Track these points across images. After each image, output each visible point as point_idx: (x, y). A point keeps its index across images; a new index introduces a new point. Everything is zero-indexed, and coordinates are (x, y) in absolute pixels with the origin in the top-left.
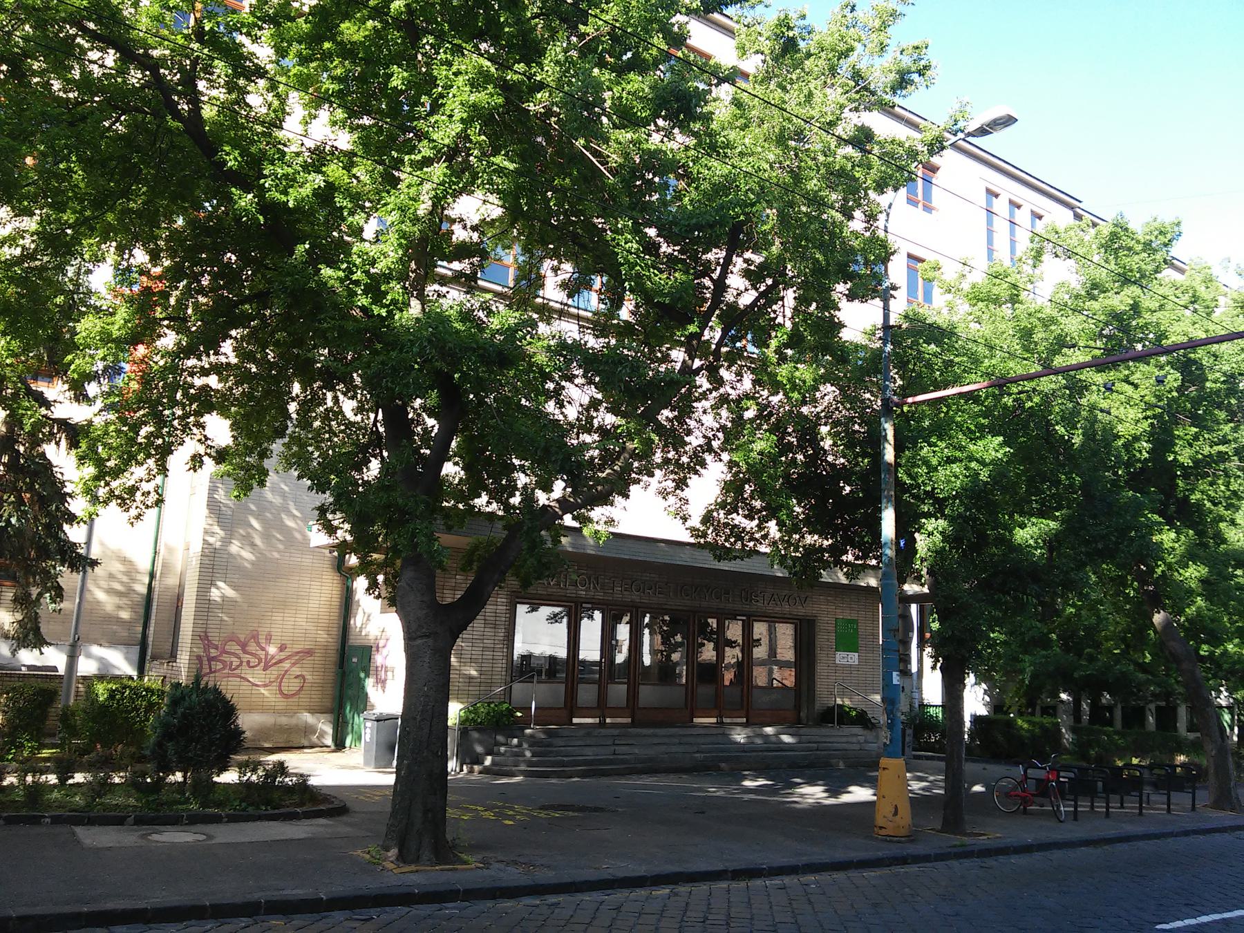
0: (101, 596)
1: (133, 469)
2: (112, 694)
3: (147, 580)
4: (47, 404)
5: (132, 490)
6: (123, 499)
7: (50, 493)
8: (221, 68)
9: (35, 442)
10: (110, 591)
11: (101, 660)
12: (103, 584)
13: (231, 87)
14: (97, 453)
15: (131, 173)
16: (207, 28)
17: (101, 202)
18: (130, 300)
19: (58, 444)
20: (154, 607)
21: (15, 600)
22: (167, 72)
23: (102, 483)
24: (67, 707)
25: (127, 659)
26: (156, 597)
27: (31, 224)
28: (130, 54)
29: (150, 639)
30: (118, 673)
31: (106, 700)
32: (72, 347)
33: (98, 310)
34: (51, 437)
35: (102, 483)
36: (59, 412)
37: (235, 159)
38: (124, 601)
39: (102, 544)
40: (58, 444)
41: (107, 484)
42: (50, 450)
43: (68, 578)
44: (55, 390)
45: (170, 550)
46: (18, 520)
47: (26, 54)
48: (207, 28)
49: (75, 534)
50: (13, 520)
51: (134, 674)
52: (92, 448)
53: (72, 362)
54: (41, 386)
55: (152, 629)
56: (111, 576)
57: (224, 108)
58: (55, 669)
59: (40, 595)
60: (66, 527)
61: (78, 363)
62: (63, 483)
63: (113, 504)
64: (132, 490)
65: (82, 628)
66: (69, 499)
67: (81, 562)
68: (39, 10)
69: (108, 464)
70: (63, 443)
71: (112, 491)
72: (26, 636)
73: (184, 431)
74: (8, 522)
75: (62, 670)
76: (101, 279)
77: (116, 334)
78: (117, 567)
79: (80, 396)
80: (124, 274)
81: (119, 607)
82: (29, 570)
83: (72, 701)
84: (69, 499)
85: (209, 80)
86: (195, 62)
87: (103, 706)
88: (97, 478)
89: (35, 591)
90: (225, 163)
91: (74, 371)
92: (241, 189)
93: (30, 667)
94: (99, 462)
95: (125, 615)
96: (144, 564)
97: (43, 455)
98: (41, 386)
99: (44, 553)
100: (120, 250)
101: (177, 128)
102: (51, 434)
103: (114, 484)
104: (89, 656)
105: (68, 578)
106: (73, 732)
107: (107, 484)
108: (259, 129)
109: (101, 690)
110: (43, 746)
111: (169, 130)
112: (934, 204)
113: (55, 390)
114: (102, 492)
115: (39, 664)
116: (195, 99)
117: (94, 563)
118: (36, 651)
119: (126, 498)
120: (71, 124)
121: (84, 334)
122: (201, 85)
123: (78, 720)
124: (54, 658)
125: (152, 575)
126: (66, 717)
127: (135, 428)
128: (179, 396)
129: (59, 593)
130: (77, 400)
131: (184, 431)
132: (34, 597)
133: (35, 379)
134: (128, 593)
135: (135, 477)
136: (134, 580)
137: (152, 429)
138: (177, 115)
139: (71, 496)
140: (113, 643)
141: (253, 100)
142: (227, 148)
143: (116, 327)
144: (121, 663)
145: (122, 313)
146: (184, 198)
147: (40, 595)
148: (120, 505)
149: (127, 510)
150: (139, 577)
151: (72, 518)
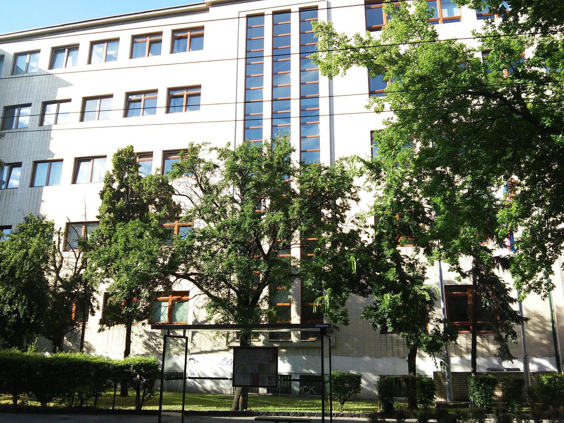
0: (532, 334)
1: (537, 274)
2: (550, 381)
3: (551, 324)
4: (490, 251)
5: (539, 284)
6: (536, 288)
7: (500, 289)
8: (531, 86)
9: (489, 269)
10: (535, 331)
11: (539, 364)
12: (532, 328)
13: (536, 91)
14: (519, 269)
15: (504, 144)
16: (520, 71)
17: (495, 160)
18: (516, 198)
19: (498, 268)
20: (558, 337)
21: (496, 339)
22: (506, 96)
23: (525, 283)
24: (529, 388)
25: (551, 363)
26: (557, 331)
27: (469, 178)
28: (489, 94)
29: (560, 353)
30: (548, 370)
31: (548, 383)
32: (498, 225)
33: (503, 206)
34: (494, 266)
35: (525, 283)
36: (495, 254)
37: (549, 122)
38: (543, 336)
39: (527, 310)
40: (498, 268)
41: (527, 283)
42: (495, 271)
43: (517, 328)
44: (490, 244)
45: (559, 309)
46: (490, 304)
47: (449, 112)
48: (520, 71)
49: (515, 307)
50: (488, 304)
51: (556, 370)
52: (517, 267)
53: (498, 231)
54: (485, 244)
55: (559, 348)
56: (534, 324)
57: (535, 102)
58: (519, 369)
59: (507, 336)
60: (510, 304)
61: (501, 231)
62: (504, 285)
63: (532, 291)
64: (539, 284)
65: (527, 349)
66: (508, 292)
67: (520, 319)
68: (451, 93)
69: (526, 273)
70: (500, 267)
71: (530, 286)
72: (504, 356)
73: (556, 252)
74: (486, 305)
75: (522, 370)
76: (499, 193)
77: (514, 215)
78: (535, 320)
79: (501, 244)
80: (511, 187)
81: (541, 339)
82: (498, 325)
83: (530, 385)
84: (508, 292)
85: (526, 92)
86: (518, 88)
87: (546, 387)
88: (522, 281)
89: (504, 335)
90: (545, 125)
91: (500, 235)
92: (555, 134)
93: (508, 369)
94: (522, 274)
95: (545, 342)
96: (548, 316)
97: (493, 274)
98: (485, 244)
99: (503, 317)
100: (506, 178)
101: (519, 118)
102: (494, 264)
103: (530, 282)
104: (533, 363)
105: (517, 328)
106: (535, 399)
107: (527, 283)
108: (555, 104)
109: (544, 378)
110: (522, 406)
111: (516, 120)
112: (185, 146)
113: (490, 244)
114: (525, 287)
115: (511, 367)
116: (522, 102)
117: (527, 319)
118: (510, 362)
119: (537, 287)
120: (475, 132)
121: (501, 218)
122: (523, 96)
123: (536, 393)
124: (519, 365)
125: (553, 322)
126: (531, 392)
127: (533, 254)
128: (549, 236)
129: (514, 335)
130: (501, 247)
131: (556, 252)
132: (504, 338)
133: (482, 242)
134: (544, 331)
135: (539, 278)
136: (546, 325)
137: (541, 254)
138: (517, 112)
139: (509, 290)
140: (543, 356)
141: (548, 93)
142: (544, 118)
143: (514, 212)
144: (548, 365)
145: (515, 205)
146: (528, 147)
147: (507, 336)
148: (535, 291)
149: (540, 293)
150: (547, 323)
151: (512, 300)
